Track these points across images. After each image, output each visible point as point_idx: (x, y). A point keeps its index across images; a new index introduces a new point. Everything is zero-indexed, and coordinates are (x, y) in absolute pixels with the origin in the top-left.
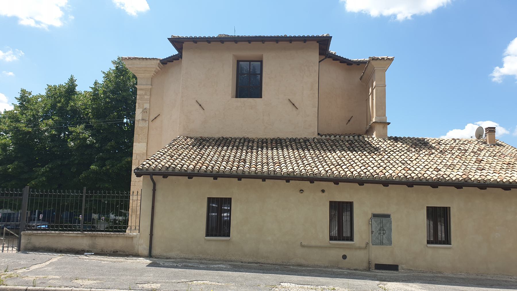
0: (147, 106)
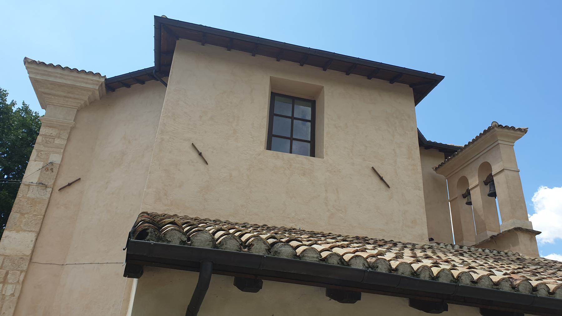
0: (56, 158)
